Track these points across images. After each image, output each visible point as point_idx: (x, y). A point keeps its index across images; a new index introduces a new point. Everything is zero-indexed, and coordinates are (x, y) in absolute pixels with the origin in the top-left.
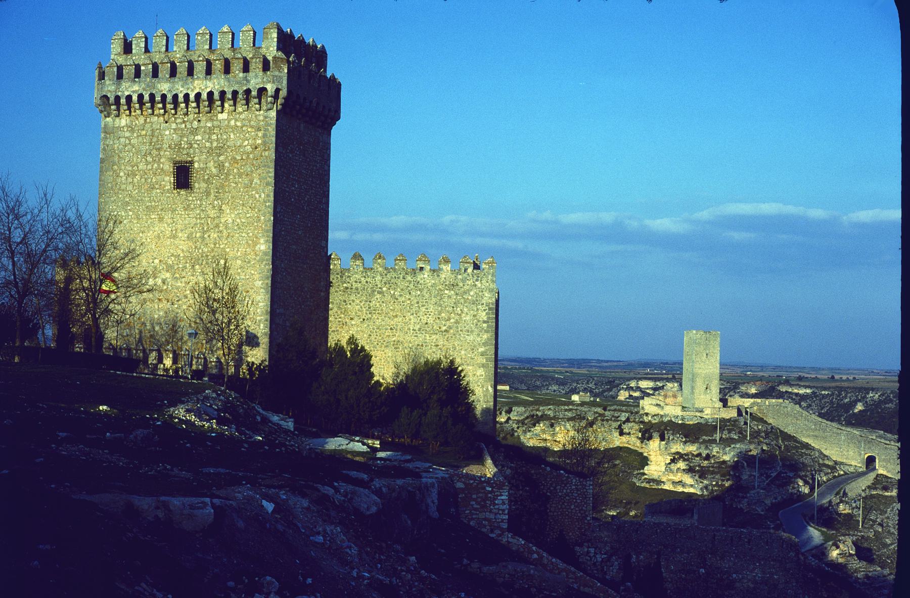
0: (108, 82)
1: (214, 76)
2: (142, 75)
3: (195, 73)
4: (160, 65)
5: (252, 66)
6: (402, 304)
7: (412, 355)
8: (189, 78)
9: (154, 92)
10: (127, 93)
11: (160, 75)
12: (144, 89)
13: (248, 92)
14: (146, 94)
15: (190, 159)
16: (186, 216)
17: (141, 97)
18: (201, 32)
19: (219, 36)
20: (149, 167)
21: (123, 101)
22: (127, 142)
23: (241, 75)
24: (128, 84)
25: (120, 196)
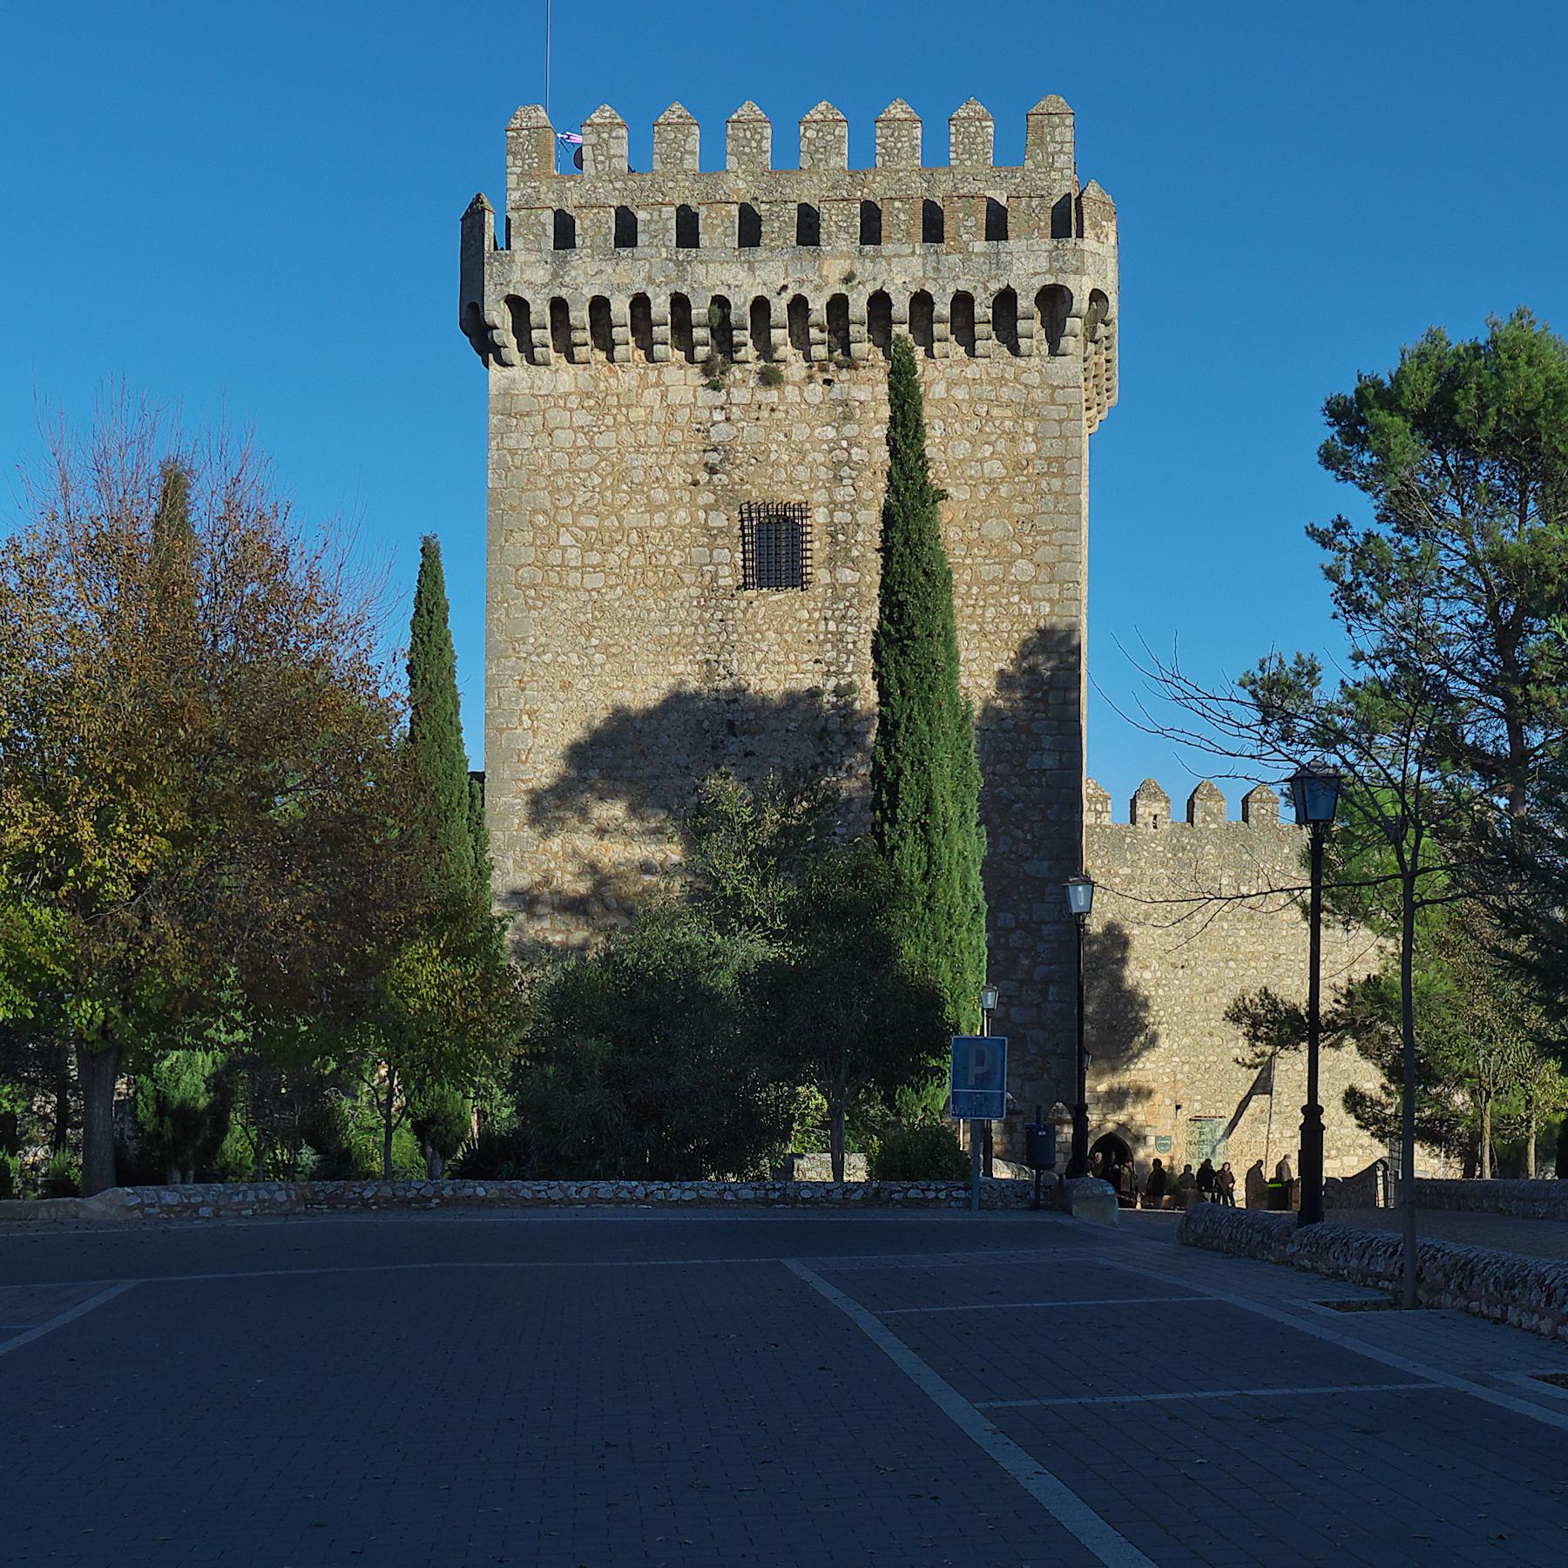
0: (520, 257)
1: (887, 248)
2: (642, 238)
3: (823, 236)
4: (703, 212)
5: (827, 226)
6: (561, 696)
7: (840, 869)
8: (625, 252)
9: (684, 291)
10: (590, 292)
11: (704, 240)
12: (650, 280)
13: (1007, 300)
14: (657, 296)
15: (799, 498)
16: (793, 668)
17: (640, 304)
18: (819, 117)
19: (879, 133)
20: (660, 519)
21: (983, 310)
22: (582, 441)
23: (980, 245)
24: (592, 268)
25: (563, 606)
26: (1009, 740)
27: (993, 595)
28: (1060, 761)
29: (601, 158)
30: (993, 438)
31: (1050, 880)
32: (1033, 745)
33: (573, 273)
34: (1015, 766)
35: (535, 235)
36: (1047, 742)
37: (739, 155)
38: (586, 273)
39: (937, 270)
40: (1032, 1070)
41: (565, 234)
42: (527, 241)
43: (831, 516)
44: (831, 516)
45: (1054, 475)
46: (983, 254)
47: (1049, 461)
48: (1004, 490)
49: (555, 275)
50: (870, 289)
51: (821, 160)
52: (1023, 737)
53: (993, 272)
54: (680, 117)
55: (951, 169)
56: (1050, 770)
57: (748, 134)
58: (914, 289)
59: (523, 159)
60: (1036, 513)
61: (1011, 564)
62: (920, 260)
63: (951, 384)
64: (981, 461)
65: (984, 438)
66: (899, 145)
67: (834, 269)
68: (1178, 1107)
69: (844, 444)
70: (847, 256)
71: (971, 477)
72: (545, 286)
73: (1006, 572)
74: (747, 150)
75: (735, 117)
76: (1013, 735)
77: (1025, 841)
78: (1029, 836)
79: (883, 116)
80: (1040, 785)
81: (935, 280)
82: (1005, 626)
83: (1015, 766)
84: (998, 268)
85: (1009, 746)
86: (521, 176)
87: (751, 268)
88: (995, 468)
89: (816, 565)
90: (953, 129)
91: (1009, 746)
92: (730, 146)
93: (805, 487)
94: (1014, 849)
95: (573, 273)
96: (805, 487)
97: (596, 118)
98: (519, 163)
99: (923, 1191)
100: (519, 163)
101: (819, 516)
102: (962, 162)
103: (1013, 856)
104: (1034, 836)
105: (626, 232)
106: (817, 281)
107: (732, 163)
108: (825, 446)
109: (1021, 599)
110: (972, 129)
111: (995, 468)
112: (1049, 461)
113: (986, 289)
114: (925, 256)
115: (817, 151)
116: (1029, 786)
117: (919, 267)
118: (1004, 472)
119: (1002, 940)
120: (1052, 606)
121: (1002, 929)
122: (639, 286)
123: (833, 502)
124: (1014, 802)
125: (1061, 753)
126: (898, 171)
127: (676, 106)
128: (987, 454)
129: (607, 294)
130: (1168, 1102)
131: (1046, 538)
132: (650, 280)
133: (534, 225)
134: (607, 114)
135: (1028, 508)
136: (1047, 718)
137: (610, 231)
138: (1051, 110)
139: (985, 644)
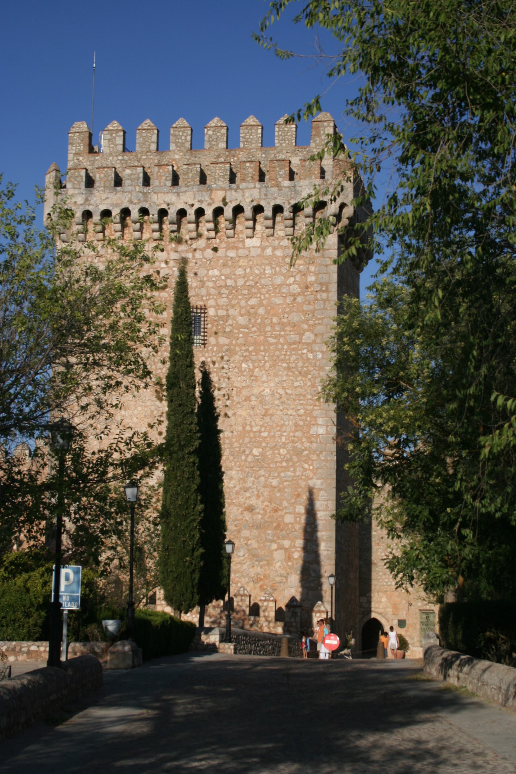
8: (119, 188)
10: (102, 207)
14: (134, 209)
18: (213, 125)
19: (241, 131)
26: (302, 420)
27: (294, 350)
28: (327, 430)
29: (112, 146)
30: (294, 274)
31: (321, 489)
32: (313, 422)
33: (95, 199)
34: (304, 433)
35: (78, 181)
36: (320, 421)
37: (176, 143)
38: (101, 199)
39: (266, 195)
40: (312, 585)
41: (90, 183)
42: (74, 184)
43: (217, 312)
44: (217, 312)
45: (323, 291)
46: (289, 187)
47: (321, 284)
48: (299, 299)
49: (87, 200)
50: (234, 204)
51: (214, 145)
52: (308, 419)
53: (293, 196)
54: (149, 126)
55: (276, 148)
56: (322, 434)
57: (181, 134)
58: (255, 204)
59: (76, 147)
60: (315, 310)
61: (303, 334)
62: (258, 190)
63: (274, 249)
64: (289, 285)
65: (290, 274)
66: (251, 137)
67: (219, 195)
68: (410, 605)
69: (223, 277)
70: (222, 189)
71: (284, 293)
72: (81, 205)
73: (301, 338)
74: (180, 141)
75: (174, 126)
76: (304, 417)
77: (309, 470)
78: (311, 467)
79: (243, 124)
80: (316, 442)
81: (265, 199)
82: (300, 364)
83: (304, 433)
84: (295, 193)
85: (301, 423)
86: (76, 154)
87: (178, 194)
88: (295, 289)
89: (209, 335)
90: (277, 129)
91: (301, 423)
92: (172, 138)
93: (204, 298)
94: (304, 473)
95: (95, 199)
96: (204, 298)
97: (110, 127)
98: (74, 148)
99: (38, 647)
100: (74, 148)
101: (211, 312)
102: (281, 144)
103: (303, 477)
104: (314, 467)
105: (118, 182)
106: (210, 201)
107: (172, 147)
108: (214, 279)
109: (308, 351)
110: (286, 129)
111: (295, 289)
112: (321, 284)
113: (289, 203)
114: (260, 189)
115: (213, 140)
116: (311, 442)
117: (258, 194)
118: (299, 290)
119: (298, 519)
120: (323, 355)
121: (298, 514)
122: (125, 205)
123: (218, 305)
124: (304, 450)
125: (327, 426)
126: (250, 149)
127: (148, 121)
128: (291, 282)
129: (110, 208)
130: (404, 602)
131: (320, 322)
132: (131, 202)
133: (77, 177)
134: (115, 125)
135: (311, 307)
136: (320, 409)
137: (82, 179)
138: (323, 119)
139: (290, 373)
